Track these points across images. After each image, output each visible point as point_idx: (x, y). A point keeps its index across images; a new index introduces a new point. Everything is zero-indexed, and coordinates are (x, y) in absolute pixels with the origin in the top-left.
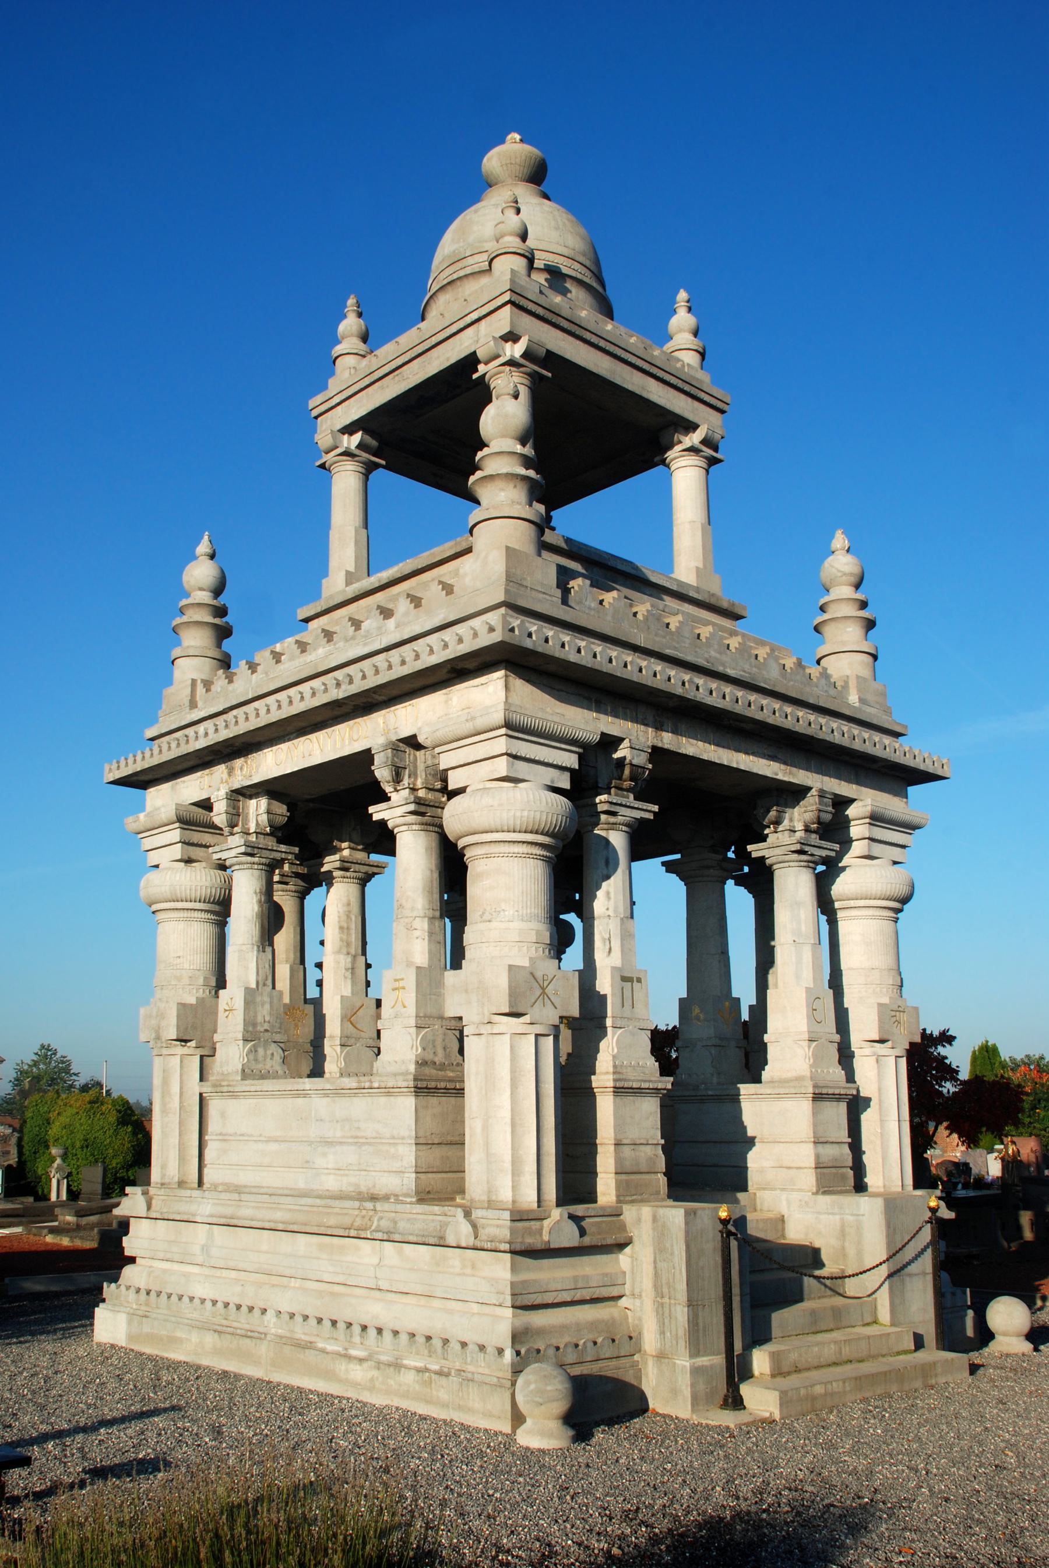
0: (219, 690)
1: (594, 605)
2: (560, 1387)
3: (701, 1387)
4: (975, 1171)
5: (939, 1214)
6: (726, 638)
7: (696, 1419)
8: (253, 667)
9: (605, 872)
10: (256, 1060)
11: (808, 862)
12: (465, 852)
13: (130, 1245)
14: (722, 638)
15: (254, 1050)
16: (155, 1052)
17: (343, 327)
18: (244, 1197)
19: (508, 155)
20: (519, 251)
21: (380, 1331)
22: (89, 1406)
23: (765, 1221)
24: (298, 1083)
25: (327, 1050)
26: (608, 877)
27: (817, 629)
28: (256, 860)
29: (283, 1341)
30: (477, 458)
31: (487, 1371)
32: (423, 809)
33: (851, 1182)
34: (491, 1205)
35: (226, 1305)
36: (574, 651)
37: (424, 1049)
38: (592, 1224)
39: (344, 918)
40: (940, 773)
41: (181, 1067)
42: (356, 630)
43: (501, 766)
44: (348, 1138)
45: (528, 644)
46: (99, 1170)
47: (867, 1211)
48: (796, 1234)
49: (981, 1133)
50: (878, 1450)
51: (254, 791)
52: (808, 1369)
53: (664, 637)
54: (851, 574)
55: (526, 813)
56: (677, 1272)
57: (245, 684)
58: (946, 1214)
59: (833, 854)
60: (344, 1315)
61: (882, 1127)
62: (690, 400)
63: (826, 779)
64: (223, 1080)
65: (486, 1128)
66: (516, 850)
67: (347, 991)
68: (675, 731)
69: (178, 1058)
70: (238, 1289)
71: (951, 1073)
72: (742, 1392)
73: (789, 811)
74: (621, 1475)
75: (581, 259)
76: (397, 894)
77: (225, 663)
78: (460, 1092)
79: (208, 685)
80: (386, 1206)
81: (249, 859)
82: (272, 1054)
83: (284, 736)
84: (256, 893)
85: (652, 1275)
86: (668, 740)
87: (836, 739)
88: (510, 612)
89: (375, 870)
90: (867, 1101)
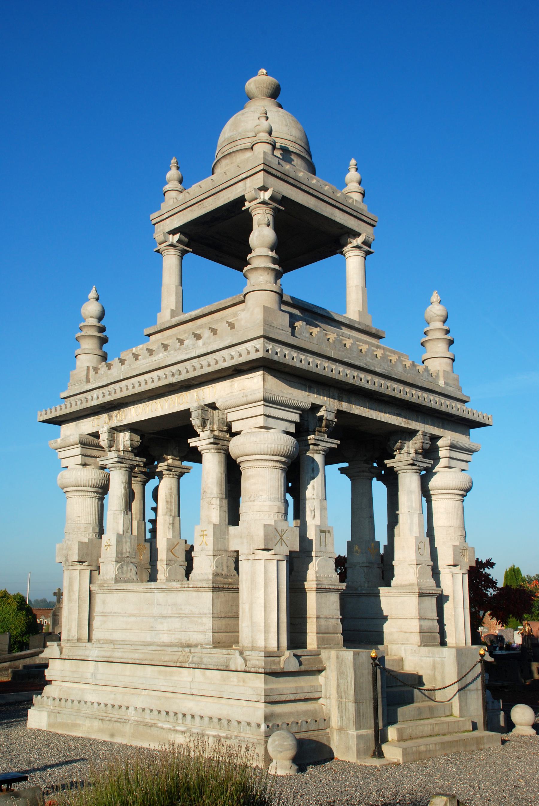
0: (103, 373)
1: (308, 335)
2: (291, 743)
3: (362, 746)
4: (506, 640)
5: (485, 658)
6: (375, 351)
7: (359, 763)
8: (122, 362)
9: (312, 475)
10: (122, 573)
11: (417, 470)
12: (241, 465)
13: (48, 674)
15: (121, 567)
16: (65, 568)
17: (169, 175)
18: (116, 646)
19: (259, 82)
20: (268, 141)
21: (193, 716)
22: (36, 759)
23: (394, 660)
24: (148, 585)
25: (159, 567)
26: (313, 478)
27: (422, 344)
28: (123, 465)
29: (138, 723)
30: (248, 258)
31: (251, 736)
32: (217, 441)
33: (438, 640)
34: (253, 649)
35: (106, 705)
36: (298, 362)
37: (217, 567)
38: (305, 659)
39: (168, 496)
40: (487, 422)
41: (80, 577)
43: (261, 421)
44: (175, 614)
45: (276, 358)
46: (7, 637)
47: (447, 655)
48: (409, 668)
49: (510, 618)
50: (454, 777)
51: (122, 428)
52: (417, 738)
53: (343, 351)
54: (441, 316)
55: (273, 446)
56: (349, 685)
57: (117, 371)
58: (489, 659)
59: (430, 466)
60: (172, 709)
61: (455, 611)
62: (356, 220)
63: (427, 426)
64: (104, 583)
65: (251, 609)
66: (268, 464)
67: (170, 536)
68: (349, 402)
69: (78, 571)
70: (112, 696)
71: (492, 583)
72: (383, 749)
73: (407, 442)
74: (324, 787)
75: (300, 142)
76: (203, 486)
77: (104, 357)
78: (237, 590)
79: (96, 370)
80: (197, 650)
81: (120, 464)
82: (131, 569)
84: (123, 483)
85: (336, 687)
86: (345, 406)
87: (433, 405)
88: (266, 341)
89: (185, 471)
90: (447, 597)
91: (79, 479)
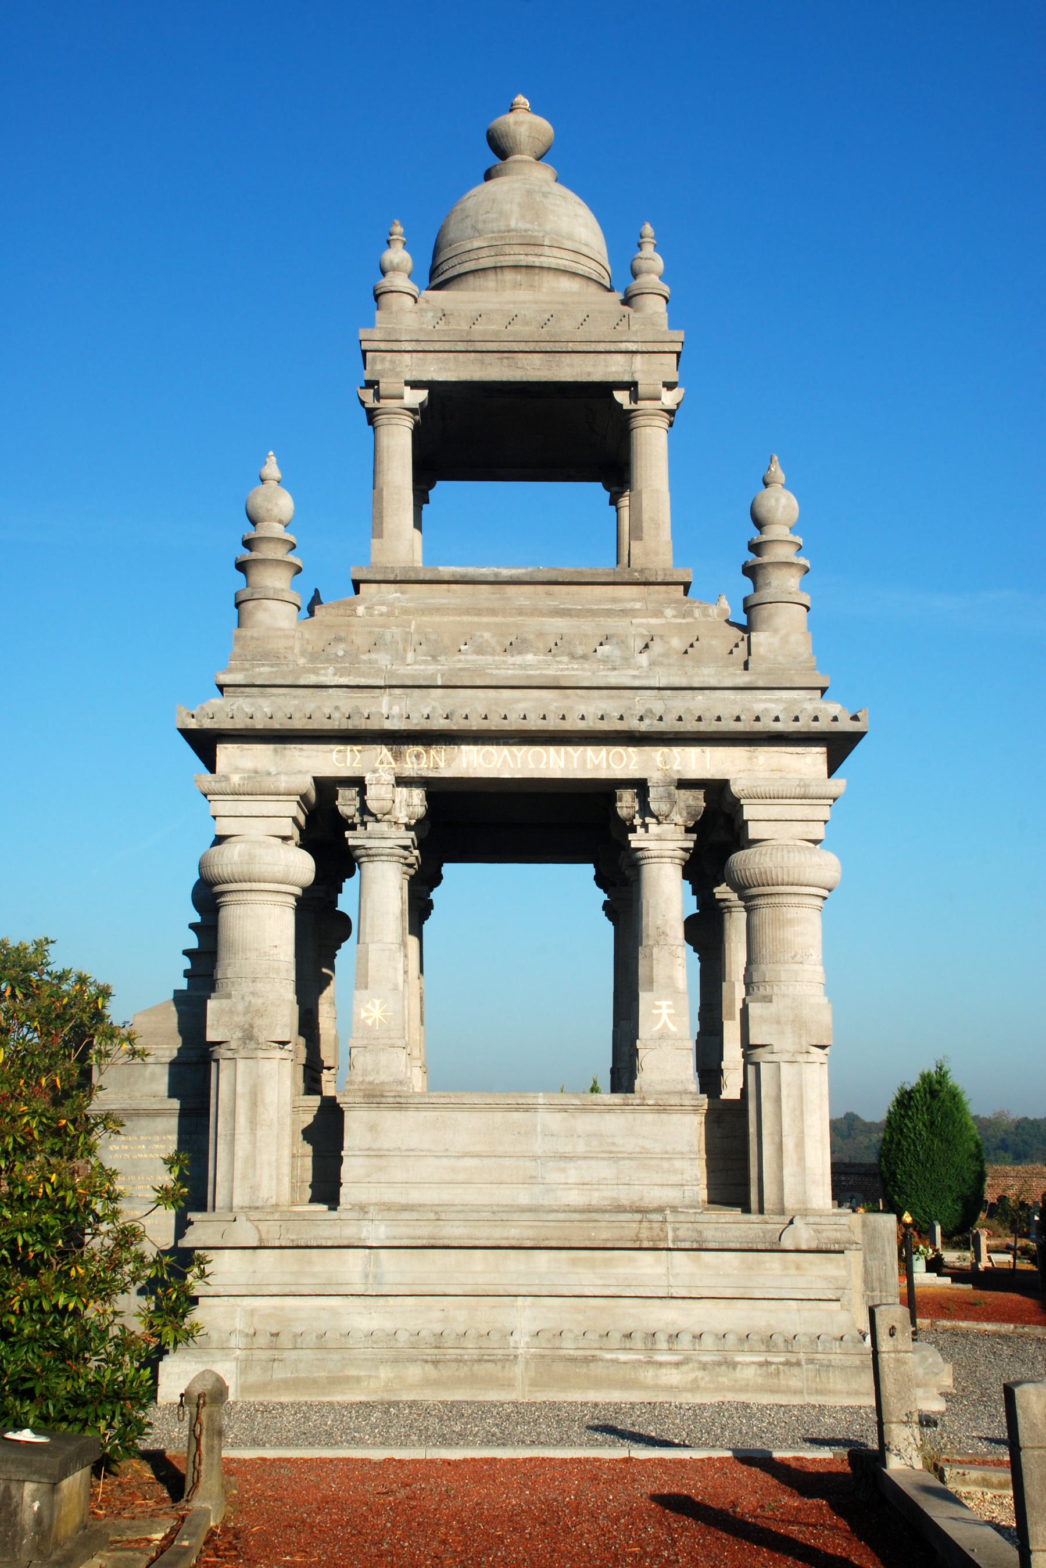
56: (889, 1268)
91: (292, 869)
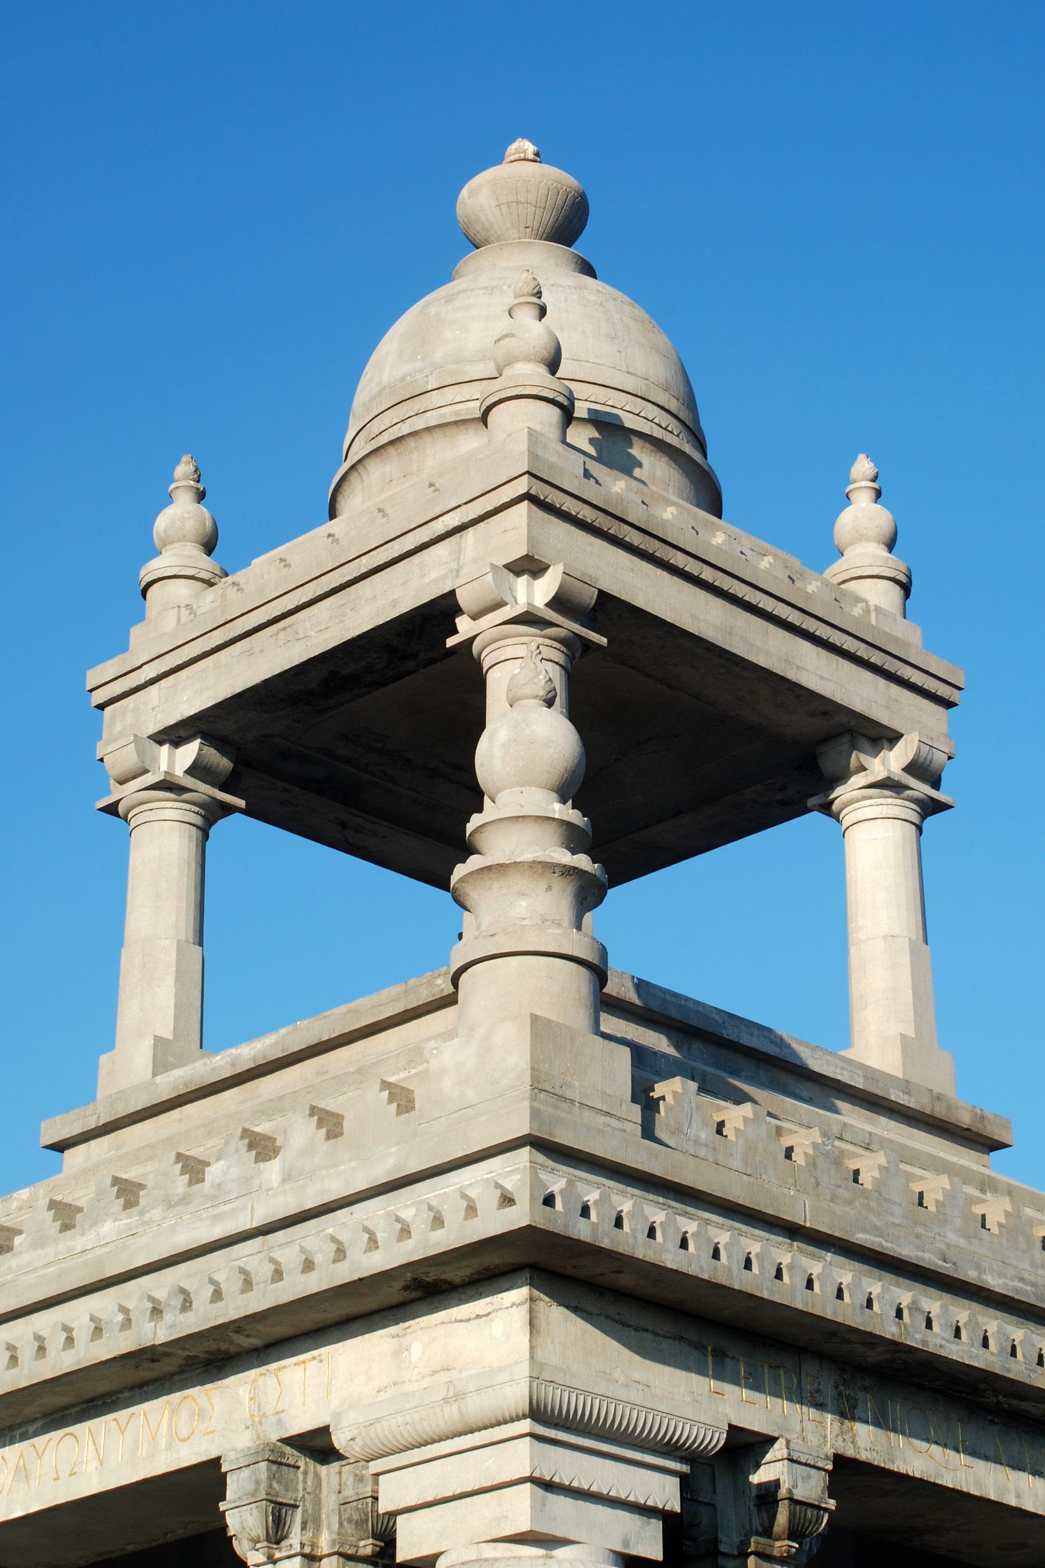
1: (707, 1134)
14: (973, 1201)
17: (163, 522)
19: (510, 185)
20: (544, 394)
30: (470, 828)
42: (191, 1183)
43: (519, 1509)
45: (581, 1231)
53: (850, 1203)
62: (881, 682)
68: (881, 1422)
83: (11, 1428)
86: (867, 1442)
88: (541, 1158)
